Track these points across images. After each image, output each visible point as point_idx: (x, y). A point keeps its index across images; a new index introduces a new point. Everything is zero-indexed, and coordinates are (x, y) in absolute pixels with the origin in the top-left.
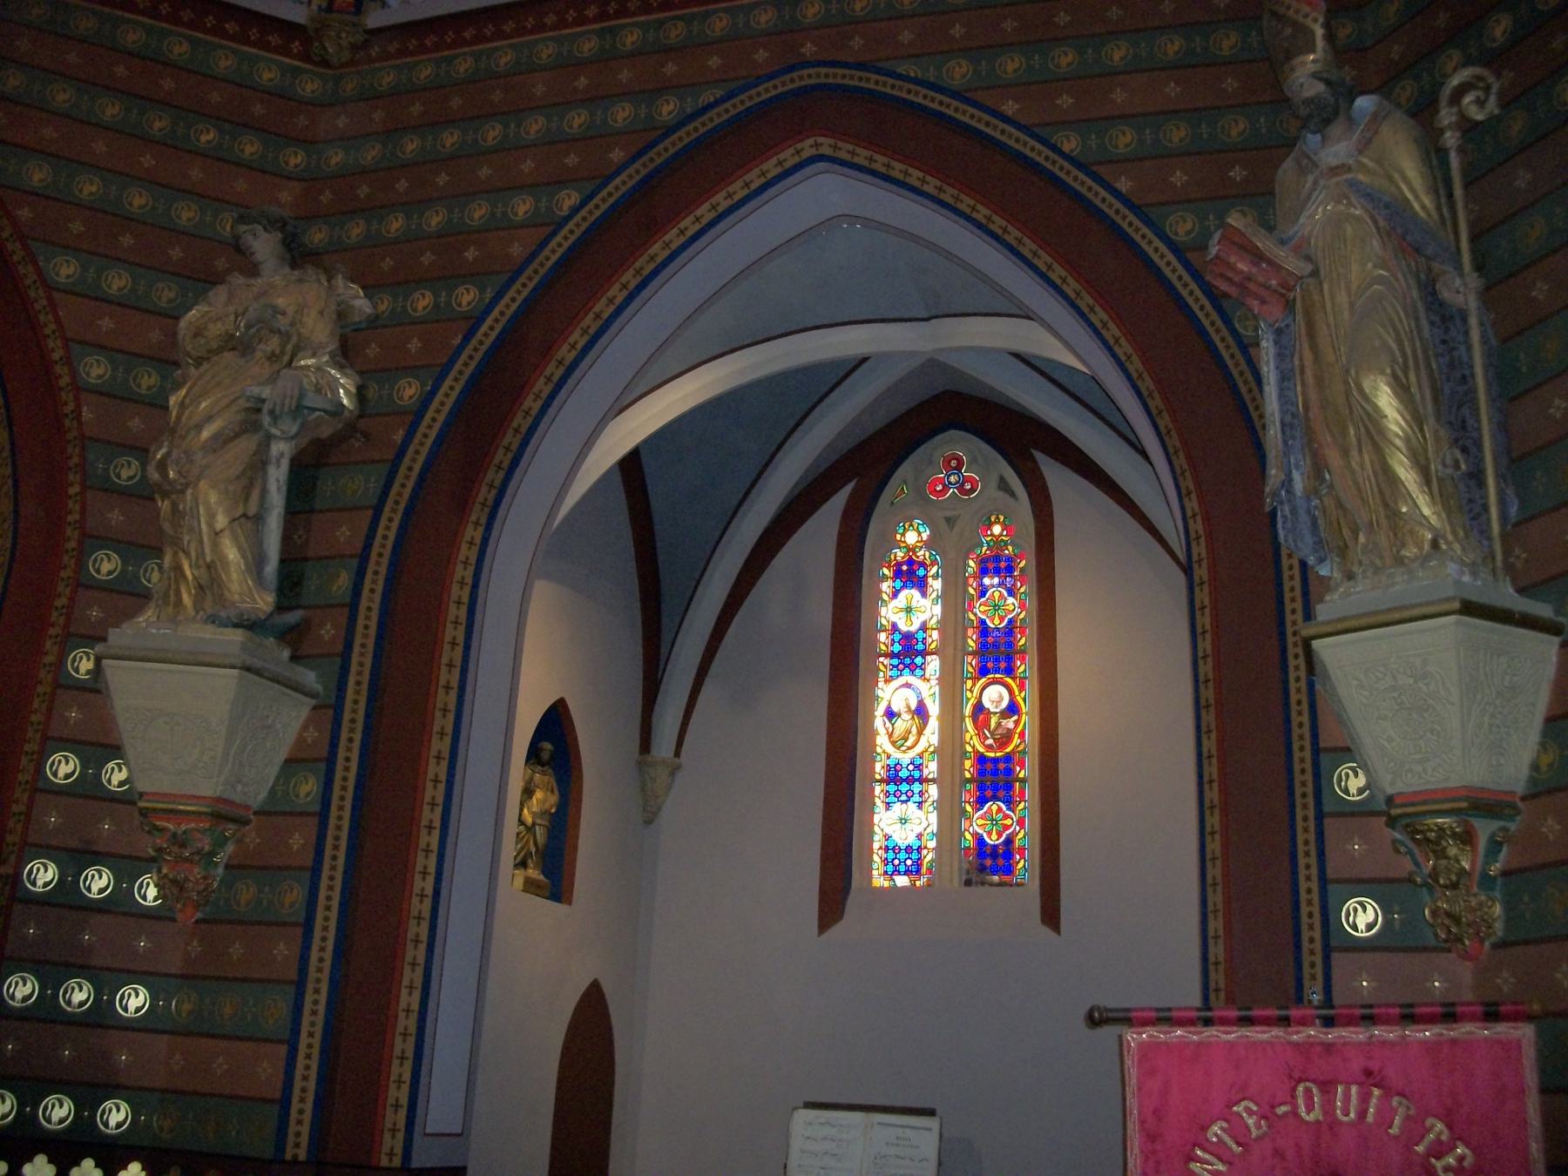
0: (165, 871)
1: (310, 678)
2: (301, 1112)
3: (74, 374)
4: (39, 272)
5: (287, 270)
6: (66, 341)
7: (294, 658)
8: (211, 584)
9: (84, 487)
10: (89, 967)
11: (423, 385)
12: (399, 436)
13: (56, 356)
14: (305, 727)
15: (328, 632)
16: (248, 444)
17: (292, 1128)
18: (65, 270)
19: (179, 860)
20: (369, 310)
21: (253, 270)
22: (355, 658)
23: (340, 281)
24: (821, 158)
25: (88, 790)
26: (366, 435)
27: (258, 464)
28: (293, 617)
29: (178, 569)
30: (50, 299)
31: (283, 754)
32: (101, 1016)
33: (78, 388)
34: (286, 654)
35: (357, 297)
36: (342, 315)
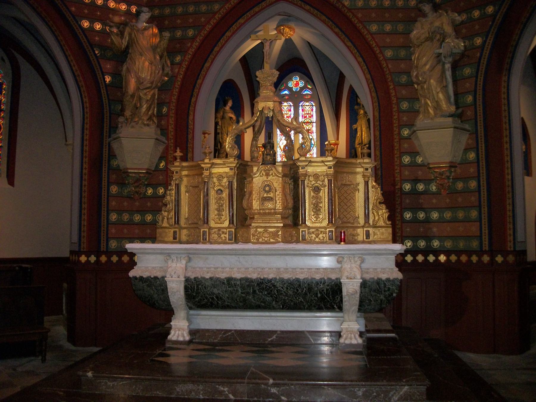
1: (467, 126)
2: (485, 238)
3: (383, 56)
4: (367, 30)
5: (435, 14)
6: (379, 47)
7: (462, 122)
8: (437, 107)
11: (483, 39)
12: (478, 55)
13: (377, 52)
14: (468, 139)
15: (469, 113)
16: (439, 67)
17: (484, 242)
18: (374, 28)
19: (442, 179)
20: (461, 20)
21: (425, 15)
22: (478, 119)
23: (449, 12)
25: (413, 165)
26: (468, 56)
27: (443, 72)
28: (460, 110)
29: (426, 104)
30: (373, 38)
31: (463, 147)
32: (427, 221)
33: (386, 59)
34: (460, 121)
35: (456, 17)
36: (453, 22)
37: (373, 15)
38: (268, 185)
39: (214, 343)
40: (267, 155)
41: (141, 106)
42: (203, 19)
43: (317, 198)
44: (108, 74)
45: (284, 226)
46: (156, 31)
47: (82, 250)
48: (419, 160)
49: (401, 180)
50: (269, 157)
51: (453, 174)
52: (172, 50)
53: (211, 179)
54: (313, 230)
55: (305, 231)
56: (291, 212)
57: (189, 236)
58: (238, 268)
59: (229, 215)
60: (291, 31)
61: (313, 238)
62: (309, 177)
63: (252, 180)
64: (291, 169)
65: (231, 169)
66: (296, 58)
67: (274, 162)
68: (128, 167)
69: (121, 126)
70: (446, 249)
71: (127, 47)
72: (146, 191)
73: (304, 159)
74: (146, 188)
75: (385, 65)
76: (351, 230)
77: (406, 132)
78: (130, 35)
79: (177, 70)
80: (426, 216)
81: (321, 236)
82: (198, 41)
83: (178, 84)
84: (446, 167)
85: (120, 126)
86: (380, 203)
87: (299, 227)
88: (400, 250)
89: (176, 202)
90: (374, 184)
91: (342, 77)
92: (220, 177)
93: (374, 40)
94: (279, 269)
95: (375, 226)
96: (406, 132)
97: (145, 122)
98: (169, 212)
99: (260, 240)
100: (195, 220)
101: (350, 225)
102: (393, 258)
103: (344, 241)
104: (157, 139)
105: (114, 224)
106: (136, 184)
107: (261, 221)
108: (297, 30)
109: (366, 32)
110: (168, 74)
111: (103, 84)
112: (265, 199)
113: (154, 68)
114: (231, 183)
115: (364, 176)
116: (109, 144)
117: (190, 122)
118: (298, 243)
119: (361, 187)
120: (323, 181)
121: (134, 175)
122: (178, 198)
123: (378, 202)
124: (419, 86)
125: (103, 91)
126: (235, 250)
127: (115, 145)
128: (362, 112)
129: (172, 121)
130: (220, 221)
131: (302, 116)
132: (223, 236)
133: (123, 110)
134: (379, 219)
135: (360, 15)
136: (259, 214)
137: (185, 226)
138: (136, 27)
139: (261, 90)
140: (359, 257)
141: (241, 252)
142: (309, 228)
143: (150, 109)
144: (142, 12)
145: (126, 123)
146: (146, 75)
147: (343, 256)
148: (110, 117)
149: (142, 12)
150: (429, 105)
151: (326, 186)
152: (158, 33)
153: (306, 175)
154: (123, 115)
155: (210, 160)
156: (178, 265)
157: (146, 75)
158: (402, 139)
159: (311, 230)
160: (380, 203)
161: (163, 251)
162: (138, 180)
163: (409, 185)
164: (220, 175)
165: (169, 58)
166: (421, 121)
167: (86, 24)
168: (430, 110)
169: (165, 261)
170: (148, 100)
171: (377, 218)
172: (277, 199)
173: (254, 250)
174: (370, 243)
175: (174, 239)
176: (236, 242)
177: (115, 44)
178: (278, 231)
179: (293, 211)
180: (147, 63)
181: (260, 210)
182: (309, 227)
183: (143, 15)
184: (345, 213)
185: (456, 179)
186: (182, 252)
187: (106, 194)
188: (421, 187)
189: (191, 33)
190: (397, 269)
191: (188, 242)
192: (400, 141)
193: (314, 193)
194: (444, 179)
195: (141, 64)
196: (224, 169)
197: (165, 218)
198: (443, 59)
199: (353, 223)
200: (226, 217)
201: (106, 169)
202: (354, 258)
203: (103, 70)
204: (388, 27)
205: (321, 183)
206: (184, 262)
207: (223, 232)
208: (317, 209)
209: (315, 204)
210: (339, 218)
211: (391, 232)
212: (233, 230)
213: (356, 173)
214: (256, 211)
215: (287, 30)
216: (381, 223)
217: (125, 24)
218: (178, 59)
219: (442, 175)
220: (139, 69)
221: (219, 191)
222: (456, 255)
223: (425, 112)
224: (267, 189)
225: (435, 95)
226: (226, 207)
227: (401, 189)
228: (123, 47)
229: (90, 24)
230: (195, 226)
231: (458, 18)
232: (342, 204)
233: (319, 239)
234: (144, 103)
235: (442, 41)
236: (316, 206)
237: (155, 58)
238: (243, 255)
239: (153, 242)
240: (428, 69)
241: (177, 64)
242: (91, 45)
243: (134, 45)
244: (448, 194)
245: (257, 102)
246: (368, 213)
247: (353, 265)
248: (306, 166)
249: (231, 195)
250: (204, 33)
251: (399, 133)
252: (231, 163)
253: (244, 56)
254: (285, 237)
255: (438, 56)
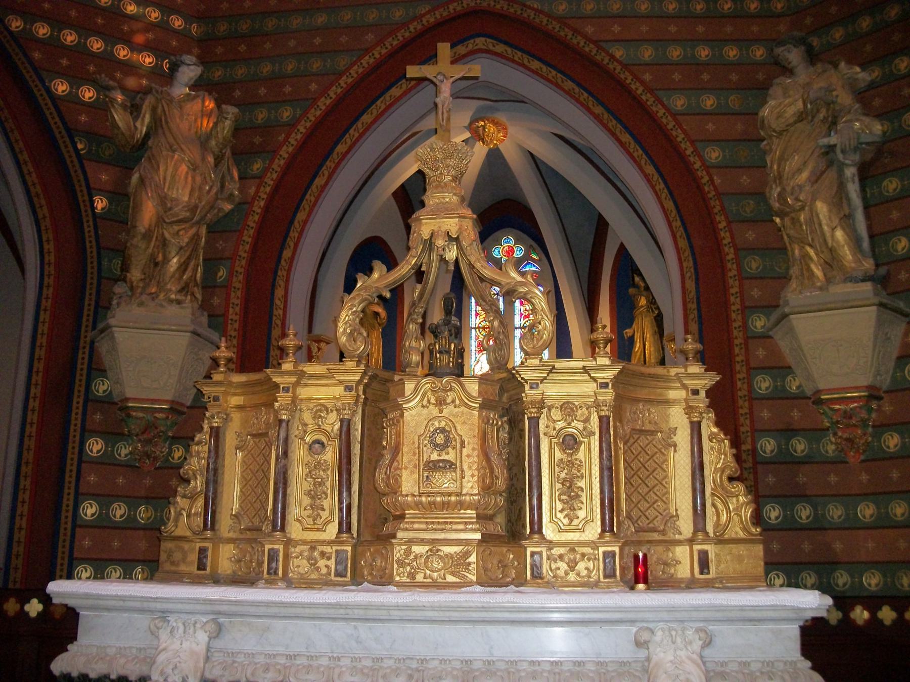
0: (840, 434)
5: (811, 69)
6: (693, 142)
8: (832, 262)
9: (729, 223)
10: (806, 496)
13: (688, 152)
16: (832, 174)
18: (679, 102)
19: (848, 426)
20: (869, 79)
21: (788, 71)
24: (487, 51)
25: (780, 396)
27: (841, 186)
29: (806, 256)
31: (895, 355)
33: (707, 167)
36: (851, 84)
37: (677, 77)
38: (443, 430)
39: (486, 515)
40: (440, 352)
41: (166, 260)
42: (313, 87)
43: (571, 464)
44: (102, 192)
45: (487, 539)
46: (210, 104)
47: (11, 586)
48: (793, 386)
49: (754, 430)
50: (445, 358)
51: (874, 415)
52: (244, 147)
53: (297, 415)
54: (562, 550)
55: (540, 553)
56: (501, 501)
57: (239, 561)
58: (354, 659)
59: (341, 510)
60: (499, 131)
61: (561, 573)
62: (550, 410)
63: (402, 416)
64: (502, 390)
65: (348, 388)
66: (509, 200)
67: (459, 371)
68: (128, 395)
69: (118, 304)
70: (865, 594)
71: (147, 136)
72: (170, 453)
73: (536, 362)
74: (171, 445)
75: (706, 179)
76: (660, 549)
77: (759, 323)
78: (154, 110)
79: (252, 191)
80: (816, 515)
81: (581, 566)
82: (302, 130)
83: (253, 220)
84: (860, 397)
85: (115, 302)
86: (731, 479)
87: (524, 542)
88: (816, 609)
89: (211, 473)
90: (715, 430)
91: (602, 226)
92: (321, 409)
93: (681, 127)
94: (468, 662)
95: (720, 541)
96: (759, 323)
97: (173, 296)
98: (192, 498)
99: (420, 578)
100: (256, 521)
101: (655, 536)
102: (793, 631)
103: (645, 581)
104: (195, 333)
105: (88, 526)
106: (145, 436)
107: (423, 526)
108: (511, 130)
109: (662, 112)
110: (232, 195)
111: (90, 212)
112: (433, 467)
113: (199, 179)
114: (346, 427)
115: (689, 410)
116: (92, 343)
117: (277, 302)
118: (521, 585)
119: (683, 438)
120: (587, 420)
121: (141, 415)
122: (215, 462)
123: (725, 478)
124: (786, 219)
125: (88, 227)
126: (346, 606)
127: (103, 347)
128: (643, 301)
129: (236, 298)
130: (314, 522)
131: (521, 314)
132: (322, 563)
133: (125, 268)
134: (729, 520)
135: (647, 77)
136: (418, 505)
137: (232, 535)
138: (169, 95)
139: (428, 193)
140: (698, 630)
141: (362, 612)
142: (551, 544)
143: (185, 270)
144: (183, 63)
145: (131, 297)
146: (182, 194)
147: (651, 625)
148: (99, 284)
149: (183, 63)
150: (811, 259)
151: (594, 434)
152: (216, 110)
153: (541, 404)
154: (124, 280)
155: (296, 364)
156: (186, 645)
157: (182, 194)
158: (750, 337)
159: (557, 551)
160: (731, 479)
161: (145, 604)
162: (149, 427)
163: (772, 442)
164: (321, 405)
165: (238, 164)
166: (793, 296)
167: (61, 88)
168: (815, 270)
169: (152, 633)
170: (181, 248)
171: (724, 518)
172: (465, 467)
173: (398, 607)
174: (708, 585)
175: (199, 569)
176: (357, 580)
177: (119, 128)
178: (467, 554)
179: (507, 500)
180: (184, 168)
181: (420, 495)
182: (551, 542)
183: (183, 69)
184: (644, 505)
185: (882, 427)
186: (199, 607)
187: (76, 457)
188: (800, 446)
189: (286, 114)
190: (808, 664)
191: (235, 581)
192: (746, 344)
193: (563, 451)
194: (855, 426)
195: (170, 170)
196: (332, 388)
197: (185, 514)
198: (840, 156)
199: (663, 532)
200: (332, 513)
201: (81, 401)
202: (684, 630)
203: (91, 181)
204: (709, 102)
205: (581, 427)
206: (202, 637)
207: (323, 554)
208: (570, 494)
209: (565, 480)
210: (629, 517)
211: (761, 554)
212: (349, 549)
213: (667, 402)
214: (409, 499)
215: (491, 128)
216: (736, 531)
217: (147, 91)
218: (257, 166)
219: (851, 418)
220: (165, 179)
221: (317, 446)
222: (894, 608)
223: (802, 274)
224: (440, 439)
225: (828, 235)
226: (330, 485)
227: (754, 450)
228: (138, 136)
229: (71, 87)
230: (255, 535)
231: (863, 76)
232: (636, 481)
233: (578, 574)
234: (173, 254)
235: (832, 124)
236: (569, 488)
237: (203, 159)
238: (367, 620)
239: (150, 578)
240: (809, 179)
241: (254, 177)
242: (68, 130)
243: (160, 131)
244: (863, 461)
245: (419, 220)
246: (704, 505)
247: (682, 653)
248: (543, 380)
249: (345, 458)
250: (315, 114)
251: (745, 326)
252: (346, 372)
253: (403, 186)
254: (486, 570)
255: (827, 153)
